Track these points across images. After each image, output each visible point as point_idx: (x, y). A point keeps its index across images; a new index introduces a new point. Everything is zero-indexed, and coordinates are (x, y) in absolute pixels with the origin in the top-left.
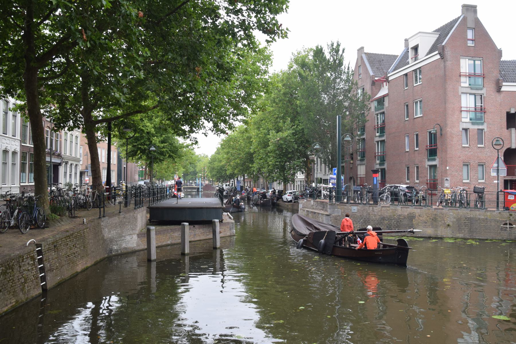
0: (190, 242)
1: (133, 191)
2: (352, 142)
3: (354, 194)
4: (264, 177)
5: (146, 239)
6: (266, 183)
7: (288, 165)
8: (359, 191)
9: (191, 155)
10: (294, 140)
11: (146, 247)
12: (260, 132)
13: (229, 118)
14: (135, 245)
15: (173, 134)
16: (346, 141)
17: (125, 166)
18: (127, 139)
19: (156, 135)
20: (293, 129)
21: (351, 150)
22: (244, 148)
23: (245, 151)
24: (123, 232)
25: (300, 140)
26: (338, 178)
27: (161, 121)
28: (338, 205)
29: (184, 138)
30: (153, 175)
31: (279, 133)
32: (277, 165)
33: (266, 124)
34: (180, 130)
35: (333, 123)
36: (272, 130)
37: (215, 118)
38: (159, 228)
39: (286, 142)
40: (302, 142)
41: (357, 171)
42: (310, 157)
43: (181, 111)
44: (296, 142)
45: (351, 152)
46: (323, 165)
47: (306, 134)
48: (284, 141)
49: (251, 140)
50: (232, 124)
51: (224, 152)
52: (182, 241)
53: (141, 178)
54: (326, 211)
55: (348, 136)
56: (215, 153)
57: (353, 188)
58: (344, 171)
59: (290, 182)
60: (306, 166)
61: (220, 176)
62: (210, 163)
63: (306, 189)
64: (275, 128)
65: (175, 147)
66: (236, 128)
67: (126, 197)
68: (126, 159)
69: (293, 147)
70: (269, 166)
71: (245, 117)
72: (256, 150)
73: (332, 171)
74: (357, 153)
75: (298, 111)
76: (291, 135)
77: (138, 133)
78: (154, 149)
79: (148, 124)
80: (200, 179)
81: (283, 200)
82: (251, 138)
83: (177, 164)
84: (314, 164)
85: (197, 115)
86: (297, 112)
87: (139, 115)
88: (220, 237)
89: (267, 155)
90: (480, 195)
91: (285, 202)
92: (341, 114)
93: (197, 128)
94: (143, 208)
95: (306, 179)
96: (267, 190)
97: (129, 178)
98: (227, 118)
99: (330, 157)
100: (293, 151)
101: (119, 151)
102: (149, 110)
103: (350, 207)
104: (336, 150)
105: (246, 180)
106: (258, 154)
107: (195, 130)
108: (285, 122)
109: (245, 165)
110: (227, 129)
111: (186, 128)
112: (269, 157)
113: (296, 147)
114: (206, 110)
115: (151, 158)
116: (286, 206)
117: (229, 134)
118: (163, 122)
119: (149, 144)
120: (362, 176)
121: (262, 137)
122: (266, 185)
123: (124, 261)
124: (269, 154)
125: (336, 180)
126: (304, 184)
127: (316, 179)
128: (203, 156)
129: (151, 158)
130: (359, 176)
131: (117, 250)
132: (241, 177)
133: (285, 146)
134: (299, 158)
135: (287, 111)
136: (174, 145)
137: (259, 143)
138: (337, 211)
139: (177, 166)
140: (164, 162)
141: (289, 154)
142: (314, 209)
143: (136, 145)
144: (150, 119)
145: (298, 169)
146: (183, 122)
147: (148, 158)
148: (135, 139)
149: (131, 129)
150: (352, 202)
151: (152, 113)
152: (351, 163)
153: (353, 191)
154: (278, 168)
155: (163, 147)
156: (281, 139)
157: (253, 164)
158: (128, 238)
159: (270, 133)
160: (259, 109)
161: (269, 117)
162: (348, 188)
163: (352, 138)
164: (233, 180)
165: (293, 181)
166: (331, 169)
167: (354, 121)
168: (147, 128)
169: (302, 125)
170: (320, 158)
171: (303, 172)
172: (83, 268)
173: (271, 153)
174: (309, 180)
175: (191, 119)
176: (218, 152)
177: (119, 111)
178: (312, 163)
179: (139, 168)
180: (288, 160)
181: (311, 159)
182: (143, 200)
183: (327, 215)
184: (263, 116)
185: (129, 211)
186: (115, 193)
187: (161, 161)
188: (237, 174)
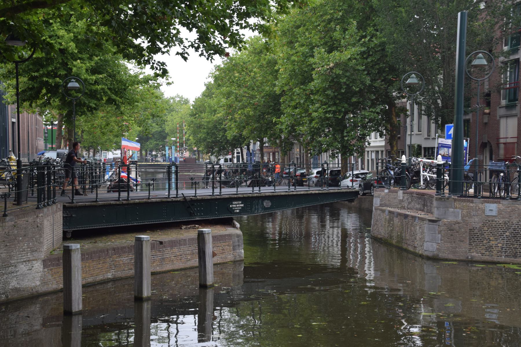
0: (153, 274)
2: (490, 68)
3: (491, 177)
4: (301, 144)
5: (61, 270)
6: (307, 156)
7: (350, 118)
9: (154, 100)
10: (364, 67)
12: (294, 51)
13: (231, 22)
14: (38, 283)
15: (115, 53)
16: (476, 66)
17: (14, 120)
18: (17, 63)
19: (80, 56)
20: (362, 45)
21: (486, 87)
23: (263, 90)
24: (11, 257)
25: (377, 67)
26: (457, 146)
27: (89, 26)
28: (455, 200)
29: (139, 63)
31: (333, 53)
32: (328, 119)
33: (307, 34)
34: (131, 47)
35: (450, 28)
36: (318, 46)
37: (203, 21)
39: (347, 71)
40: (381, 71)
42: (396, 102)
43: (130, 6)
44: (368, 71)
46: (425, 118)
48: (343, 70)
49: (276, 68)
50: (238, 34)
51: (221, 93)
53: (49, 146)
54: (430, 212)
55: (480, 55)
56: (204, 95)
57: (489, 165)
58: (468, 131)
59: (355, 154)
60: (389, 120)
61: (213, 142)
62: (193, 115)
63: (387, 168)
64: (326, 43)
65: (121, 81)
66: (245, 43)
69: (363, 83)
70: (311, 121)
71: (263, 19)
72: (285, 89)
73: (443, 130)
74: (499, 92)
76: (358, 57)
78: (77, 85)
79: (62, 32)
80: (173, 148)
82: (276, 63)
84: (406, 116)
85: (164, 14)
87: (39, 11)
88: (214, 265)
92: (468, 8)
94: (54, 206)
95: (389, 148)
96: (308, 171)
97: (24, 144)
99: (439, 101)
103: (481, 206)
104: (453, 86)
105: (265, 150)
106: (291, 96)
107: (161, 46)
108: (347, 30)
109: (263, 119)
111: (143, 42)
112: (313, 103)
113: (368, 82)
115: (70, 103)
117: (231, 55)
118: (94, 28)
119: (66, 75)
120: (509, 140)
122: (307, 160)
123: (13, 317)
124: (312, 97)
125: (450, 150)
126: (384, 157)
127: (409, 147)
128: (179, 101)
130: (502, 141)
133: (345, 80)
135: (350, 6)
137: (293, 75)
138: (453, 212)
139: (125, 120)
141: (352, 96)
142: (403, 208)
143: (37, 77)
144: (66, 22)
145: (372, 126)
147: (64, 104)
148: (34, 64)
149: (23, 41)
150: (487, 194)
151: (68, 9)
152: (486, 114)
153: (488, 172)
154: (331, 126)
155: (96, 82)
156: (337, 65)
157: (279, 118)
158: (23, 268)
159: (316, 54)
161: (313, 19)
162: (477, 167)
163: (490, 61)
164: (239, 150)
165: (361, 152)
166: (441, 127)
167: (497, 23)
168: (59, 41)
170: (418, 103)
172: (47, 290)
173: (316, 94)
174: (395, 149)
175: (152, 23)
176: (209, 93)
178: (402, 115)
180: (351, 108)
181: (399, 106)
183: (430, 221)
184: (300, 17)
185: (25, 213)
187: (92, 110)
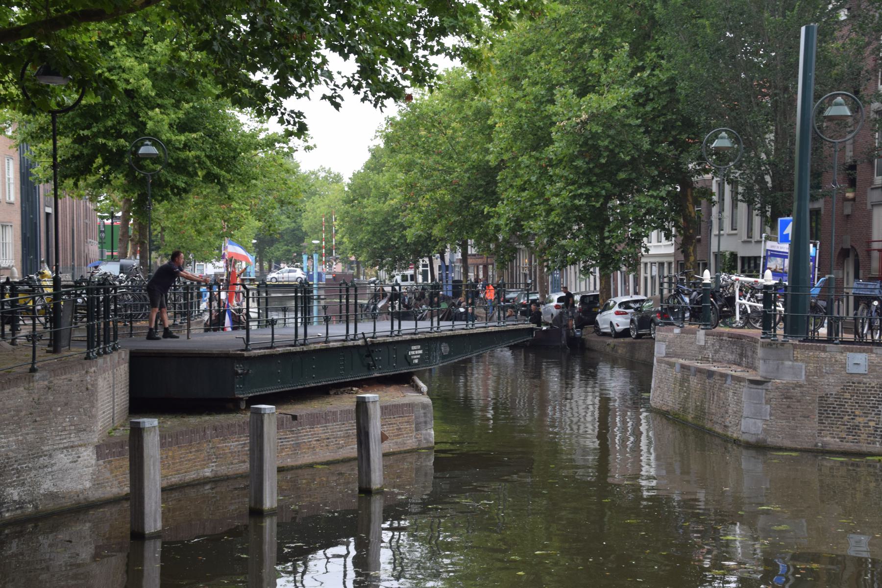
0: (280, 470)
1: (79, 296)
2: (856, 122)
3: (856, 308)
4: (532, 251)
5: (126, 463)
6: (541, 270)
7: (616, 207)
8: (875, 298)
9: (284, 175)
11: (127, 489)
12: (520, 93)
13: (415, 43)
14: (88, 485)
15: (218, 97)
16: (831, 118)
17: (49, 210)
18: (54, 113)
19: (159, 101)
21: (849, 154)
22: (465, 148)
23: (468, 159)
24: (42, 440)
25: (662, 119)
26: (798, 254)
27: (174, 51)
28: (795, 347)
29: (260, 113)
30: (151, 241)
32: (578, 208)
33: (542, 64)
35: (786, 55)
36: (561, 85)
38: (173, 423)
39: (610, 127)
40: (668, 127)
41: (869, 226)
42: (694, 179)
43: (244, 17)
44: (647, 127)
45: (849, 161)
46: (743, 207)
47: (681, 98)
48: (603, 125)
49: (489, 122)
50: (426, 63)
52: (252, 466)
53: (108, 253)
54: (752, 367)
55: (839, 99)
56: (367, 167)
57: (853, 287)
59: (624, 269)
61: (383, 248)
62: (348, 201)
63: (679, 292)
64: (574, 80)
65: (228, 144)
66: (439, 78)
67: (54, 316)
68: (50, 186)
69: (636, 147)
70: (549, 212)
71: (469, 38)
73: (773, 228)
74: (871, 163)
75: (657, 16)
76: (629, 104)
77: (96, 91)
78: (153, 150)
79: (129, 62)
80: (316, 256)
81: (597, 330)
82: (489, 114)
83: (234, 205)
84: (711, 203)
85: (301, 30)
86: (652, 18)
87: (92, 26)
89: (543, 172)
90: (464, 316)
91: (605, 334)
92: (818, 20)
93: (303, 79)
94: (115, 355)
95: (681, 257)
96: (543, 296)
97: (65, 250)
98: (408, 42)
99: (768, 178)
100: (633, 159)
101: (27, 154)
102: (132, 10)
103: (839, 357)
104: (792, 152)
105: (470, 261)
106: (514, 170)
107: (296, 84)
108: (611, 56)
109: (468, 207)
110: (407, 83)
111: (266, 78)
112: (552, 182)
113: (646, 146)
114: (333, 16)
116: (608, 349)
118: (183, 54)
119: (136, 135)
121: (527, 112)
125: (787, 261)
127: (716, 255)
128: (325, 178)
129: (141, 183)
131: (21, 504)
132: (454, 251)
133: (606, 143)
134: (655, 184)
135: (616, 17)
136: (223, 137)
137: (518, 134)
138: (792, 367)
139: (234, 209)
140: (191, 195)
141: (619, 170)
142: (706, 360)
144: (136, 45)
145: (653, 221)
146: (253, 55)
147: (134, 182)
148: (82, 115)
149: (66, 77)
150: (850, 337)
151: (140, 23)
152: (847, 200)
153: (851, 299)
155: (187, 146)
156: (593, 117)
157: (495, 205)
158: (63, 459)
159: (558, 97)
160: (518, 12)
161: (554, 39)
162: (833, 289)
163: (855, 109)
164: (427, 260)
165: (634, 265)
166: (771, 222)
167: (868, 44)
168: (125, 76)
169: (669, 65)
171: (670, 231)
173: (557, 166)
174: (692, 259)
176: (375, 164)
177: (15, 9)
178: (704, 202)
179: (102, 218)
182: (115, 326)
183: (752, 382)
185: (66, 367)
186: (13, 303)
187: (181, 192)
188: (442, 239)
